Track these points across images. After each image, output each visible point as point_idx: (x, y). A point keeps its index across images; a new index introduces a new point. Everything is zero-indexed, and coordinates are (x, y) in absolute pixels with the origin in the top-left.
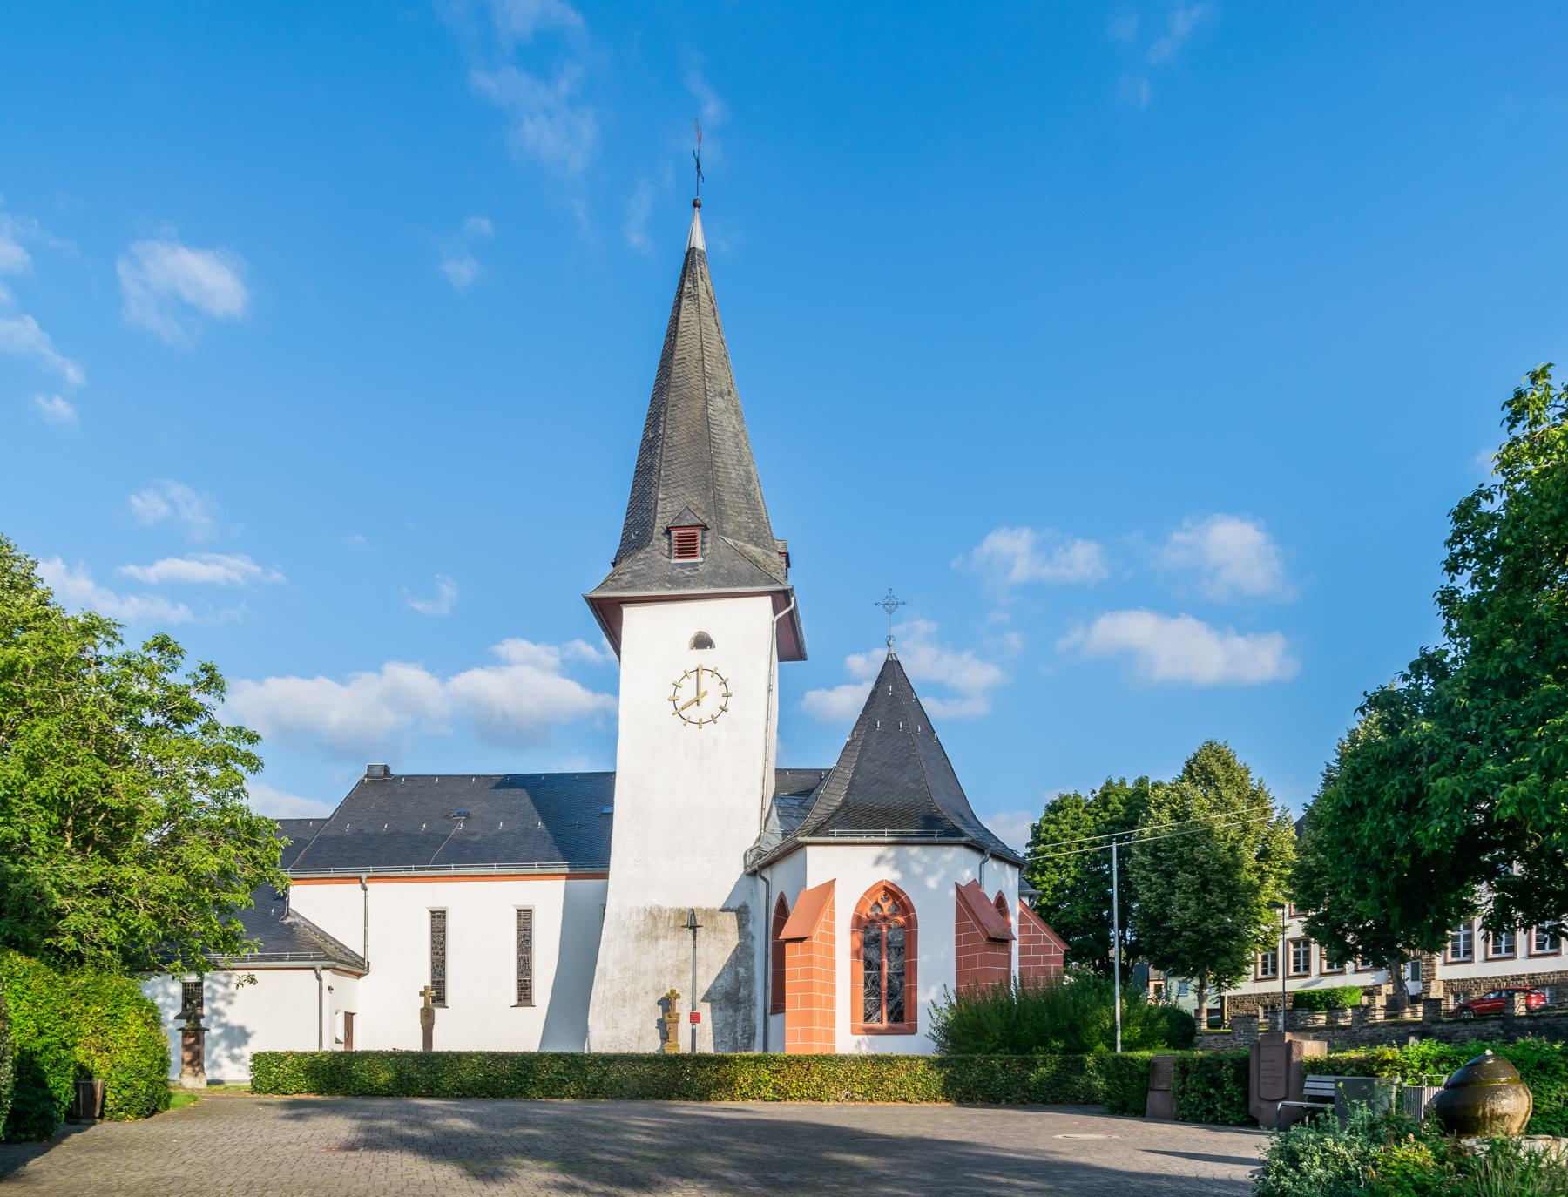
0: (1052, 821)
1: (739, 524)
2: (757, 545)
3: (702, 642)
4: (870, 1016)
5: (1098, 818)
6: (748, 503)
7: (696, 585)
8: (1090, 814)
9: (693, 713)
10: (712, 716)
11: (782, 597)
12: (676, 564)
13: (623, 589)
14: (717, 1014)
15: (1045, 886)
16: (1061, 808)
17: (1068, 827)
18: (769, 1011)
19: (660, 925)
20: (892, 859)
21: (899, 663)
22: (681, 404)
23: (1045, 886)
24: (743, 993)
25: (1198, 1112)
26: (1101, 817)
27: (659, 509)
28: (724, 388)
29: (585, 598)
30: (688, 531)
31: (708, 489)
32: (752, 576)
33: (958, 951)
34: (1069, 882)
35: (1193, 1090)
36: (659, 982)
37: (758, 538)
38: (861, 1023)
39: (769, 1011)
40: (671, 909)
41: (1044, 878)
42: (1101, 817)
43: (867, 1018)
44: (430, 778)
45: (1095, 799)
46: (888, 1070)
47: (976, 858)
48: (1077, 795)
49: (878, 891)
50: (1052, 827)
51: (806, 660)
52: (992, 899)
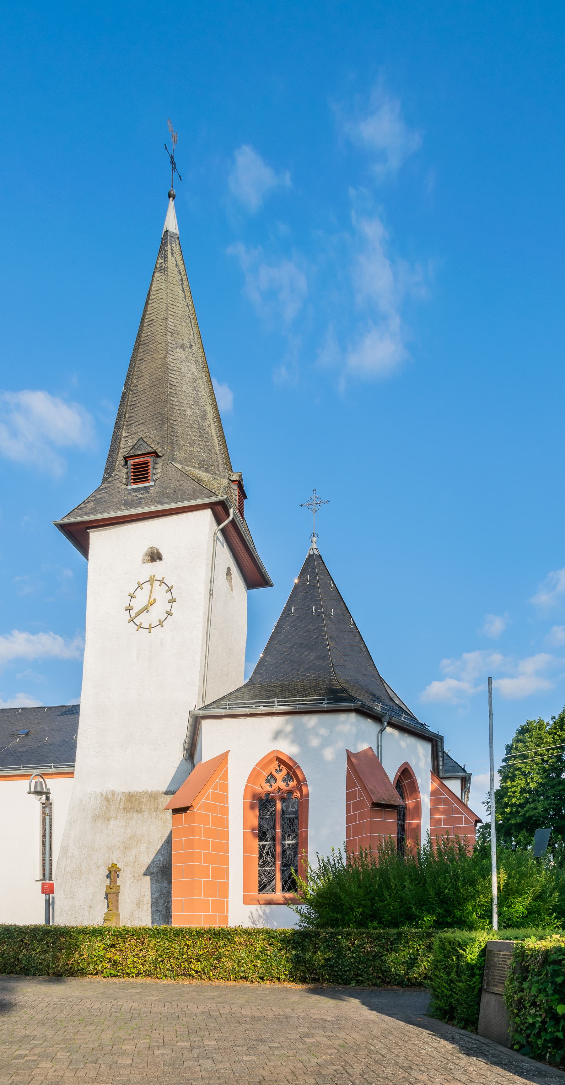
0: (521, 741)
1: (191, 454)
2: (207, 471)
3: (155, 556)
4: (265, 886)
5: (556, 736)
6: (201, 436)
7: (147, 505)
8: (550, 734)
9: (144, 619)
10: (160, 621)
11: (219, 508)
12: (132, 490)
13: (86, 514)
14: (154, 885)
15: (514, 789)
16: (528, 731)
17: (533, 744)
19: (113, 808)
20: (291, 733)
21: (320, 556)
22: (147, 358)
23: (514, 789)
25: (540, 1042)
26: (558, 736)
27: (122, 446)
28: (186, 342)
29: (56, 525)
30: (142, 459)
31: (163, 424)
32: (194, 492)
33: (349, 820)
34: (533, 785)
35: (534, 1004)
36: (109, 857)
37: (209, 465)
38: (255, 893)
40: (123, 793)
41: (514, 783)
42: (558, 736)
43: (262, 888)
44: (16, 710)
45: (555, 723)
46: (225, 945)
47: (370, 726)
48: (540, 721)
49: (270, 762)
50: (520, 745)
52: (392, 774)
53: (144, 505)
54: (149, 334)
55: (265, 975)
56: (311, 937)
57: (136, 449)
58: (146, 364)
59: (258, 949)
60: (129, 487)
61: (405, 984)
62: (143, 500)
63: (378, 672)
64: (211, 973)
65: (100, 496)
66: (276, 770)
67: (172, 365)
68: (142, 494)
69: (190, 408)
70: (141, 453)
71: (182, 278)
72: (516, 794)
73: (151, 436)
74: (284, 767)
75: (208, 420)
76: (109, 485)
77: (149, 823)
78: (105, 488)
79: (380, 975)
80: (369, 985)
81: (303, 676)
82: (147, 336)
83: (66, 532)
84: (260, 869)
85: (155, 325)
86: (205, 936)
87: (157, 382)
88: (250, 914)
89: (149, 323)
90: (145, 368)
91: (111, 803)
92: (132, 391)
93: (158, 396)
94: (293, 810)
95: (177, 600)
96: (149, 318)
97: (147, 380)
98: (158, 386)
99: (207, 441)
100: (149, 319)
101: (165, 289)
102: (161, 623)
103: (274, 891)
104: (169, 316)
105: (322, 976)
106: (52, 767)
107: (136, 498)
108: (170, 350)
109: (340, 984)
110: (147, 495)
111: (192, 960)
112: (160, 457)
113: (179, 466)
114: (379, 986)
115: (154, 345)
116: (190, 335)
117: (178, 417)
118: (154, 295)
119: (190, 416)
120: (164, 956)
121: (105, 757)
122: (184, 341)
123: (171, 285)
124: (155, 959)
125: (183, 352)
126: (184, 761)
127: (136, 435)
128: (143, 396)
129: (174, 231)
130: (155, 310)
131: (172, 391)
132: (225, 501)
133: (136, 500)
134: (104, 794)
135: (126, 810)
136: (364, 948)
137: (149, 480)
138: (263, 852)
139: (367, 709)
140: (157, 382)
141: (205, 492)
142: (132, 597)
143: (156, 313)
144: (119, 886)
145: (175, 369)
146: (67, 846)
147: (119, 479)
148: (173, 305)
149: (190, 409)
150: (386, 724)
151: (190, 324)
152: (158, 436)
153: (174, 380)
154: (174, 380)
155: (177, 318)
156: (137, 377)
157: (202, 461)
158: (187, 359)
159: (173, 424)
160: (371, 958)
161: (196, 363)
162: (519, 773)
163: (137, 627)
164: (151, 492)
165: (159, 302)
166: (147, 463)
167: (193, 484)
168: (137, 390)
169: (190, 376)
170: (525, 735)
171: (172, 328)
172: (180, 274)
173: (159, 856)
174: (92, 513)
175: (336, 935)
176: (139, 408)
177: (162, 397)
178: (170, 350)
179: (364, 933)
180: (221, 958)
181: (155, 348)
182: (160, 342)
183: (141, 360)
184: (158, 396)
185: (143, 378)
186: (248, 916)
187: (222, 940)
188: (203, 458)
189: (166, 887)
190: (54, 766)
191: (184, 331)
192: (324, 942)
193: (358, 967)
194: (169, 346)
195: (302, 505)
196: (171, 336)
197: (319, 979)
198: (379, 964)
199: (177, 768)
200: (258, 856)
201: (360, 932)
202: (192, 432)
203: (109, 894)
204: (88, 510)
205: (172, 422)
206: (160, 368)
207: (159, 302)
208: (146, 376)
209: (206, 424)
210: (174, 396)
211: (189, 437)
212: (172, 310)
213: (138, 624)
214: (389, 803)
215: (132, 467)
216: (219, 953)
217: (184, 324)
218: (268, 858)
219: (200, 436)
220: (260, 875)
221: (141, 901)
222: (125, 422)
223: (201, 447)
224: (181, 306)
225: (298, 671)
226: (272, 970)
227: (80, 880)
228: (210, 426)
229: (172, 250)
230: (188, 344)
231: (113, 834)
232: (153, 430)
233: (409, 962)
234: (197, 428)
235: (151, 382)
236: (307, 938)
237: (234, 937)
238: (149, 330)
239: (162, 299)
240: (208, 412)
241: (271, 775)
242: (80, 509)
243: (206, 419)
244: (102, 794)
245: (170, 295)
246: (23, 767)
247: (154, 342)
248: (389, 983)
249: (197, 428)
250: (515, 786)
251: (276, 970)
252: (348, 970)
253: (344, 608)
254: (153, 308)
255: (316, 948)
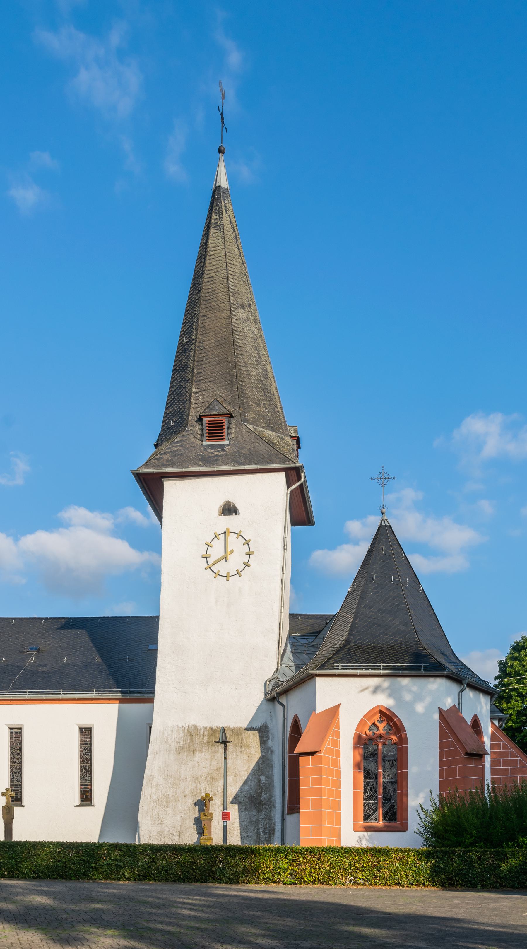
0: (516, 659)
1: (258, 413)
2: (273, 430)
4: (369, 816)
6: (265, 395)
10: (237, 571)
11: (293, 473)
13: (164, 466)
14: (243, 814)
15: (511, 711)
18: (286, 812)
19: (196, 741)
20: (387, 688)
22: (210, 315)
23: (511, 711)
24: (264, 796)
27: (193, 401)
30: (216, 419)
31: (232, 384)
33: (441, 764)
36: (196, 787)
38: (361, 822)
39: (286, 812)
40: (205, 728)
41: (510, 705)
46: (384, 860)
47: (455, 688)
50: (516, 663)
51: (313, 525)
52: (469, 721)
53: (221, 463)
54: (210, 290)
55: (414, 882)
56: (450, 854)
57: (211, 409)
58: (209, 321)
59: (410, 863)
60: (205, 443)
61: (516, 887)
62: (220, 458)
63: (444, 632)
64: (373, 880)
65: (175, 449)
66: (378, 720)
67: (236, 326)
68: (218, 451)
69: (255, 368)
70: (216, 413)
71: (236, 235)
72: (513, 717)
73: (222, 395)
74: (385, 719)
75: (269, 379)
76: (184, 438)
77: (234, 756)
78: (180, 441)
79: (499, 881)
80: (490, 887)
81: (392, 640)
82: (208, 293)
83: (141, 481)
84: (364, 802)
85: (215, 283)
86: (369, 853)
87: (223, 342)
88: (359, 839)
89: (209, 280)
90: (209, 325)
91: (194, 737)
92: (198, 347)
93: (225, 356)
94: (393, 754)
95: (255, 553)
96: (208, 274)
97: (212, 338)
98: (224, 345)
99: (271, 400)
100: (209, 276)
101: (223, 247)
102: (239, 573)
103: (377, 820)
104: (229, 275)
105: (457, 881)
106: (95, 692)
107: (213, 455)
108: (233, 311)
109: (469, 887)
110: (223, 453)
111: (358, 871)
112: (233, 417)
113: (251, 427)
114: (498, 888)
115: (217, 303)
116: (247, 293)
117: (246, 378)
118: (212, 251)
119: (255, 376)
120: (336, 868)
121: (186, 693)
122: (244, 300)
123: (228, 244)
124: (329, 870)
125: (244, 311)
126: (265, 702)
127: (207, 392)
128: (209, 353)
129: (226, 187)
130: (214, 267)
131: (238, 352)
132: (300, 468)
133: (213, 457)
134: (187, 728)
135: (210, 744)
136: (488, 861)
137: (224, 439)
138: (367, 788)
139: (455, 676)
140: (223, 342)
141: (280, 456)
142: (246, 565)
143: (215, 270)
144: (212, 814)
145: (239, 329)
146: (151, 776)
147: (194, 435)
148: (231, 264)
149: (254, 369)
150: (465, 685)
151: (247, 282)
152: (229, 395)
153: (239, 341)
154: (239, 341)
155: (236, 277)
156: (201, 333)
157: (268, 420)
158: (247, 318)
159: (242, 385)
160: (492, 869)
161: (255, 322)
162: (516, 694)
163: (214, 574)
164: (227, 450)
165: (217, 259)
166: (222, 423)
167: (268, 447)
168: (202, 346)
169: (252, 336)
170: (521, 652)
171: (233, 288)
172: (234, 231)
173: (247, 787)
174: (169, 465)
175: (467, 852)
176: (207, 365)
177: (231, 358)
178: (233, 311)
179: (488, 851)
180: (381, 869)
181: (217, 306)
182: (222, 301)
183: (204, 316)
184: (225, 356)
185: (209, 335)
186: (356, 840)
187: (382, 856)
188: (269, 417)
189: (255, 815)
190: (96, 691)
191: (243, 290)
192: (459, 857)
193: (483, 875)
194: (232, 307)
195: (372, 479)
196: (233, 297)
197: (454, 884)
198: (498, 873)
199: (258, 707)
200: (363, 791)
201: (485, 850)
202: (258, 392)
203: (204, 820)
204: (165, 462)
205: (241, 383)
206: (225, 328)
207: (217, 259)
208: (211, 334)
209: (268, 383)
210: (241, 357)
211: (256, 397)
212: (231, 269)
213: (216, 571)
214: (478, 753)
215: (207, 425)
216: (380, 866)
217: (242, 283)
218: (372, 793)
219: (264, 396)
220: (365, 807)
221: (231, 828)
222: (194, 378)
223: (266, 406)
224: (238, 264)
225: (386, 634)
226: (420, 877)
227: (167, 807)
228: (271, 385)
229: (226, 207)
230: (247, 303)
231: (199, 765)
232: (223, 389)
233: (520, 871)
234: (261, 388)
235: (217, 341)
236: (446, 854)
237: (391, 854)
238: (210, 287)
239: (220, 257)
240: (269, 371)
241: (374, 724)
242: (157, 459)
243: (268, 378)
244: (184, 728)
245: (228, 254)
246: (62, 692)
247: (216, 299)
248: (504, 886)
249: (261, 388)
250: (510, 708)
251: (423, 878)
252: (476, 877)
253: (414, 575)
254: (211, 265)
255: (453, 861)
